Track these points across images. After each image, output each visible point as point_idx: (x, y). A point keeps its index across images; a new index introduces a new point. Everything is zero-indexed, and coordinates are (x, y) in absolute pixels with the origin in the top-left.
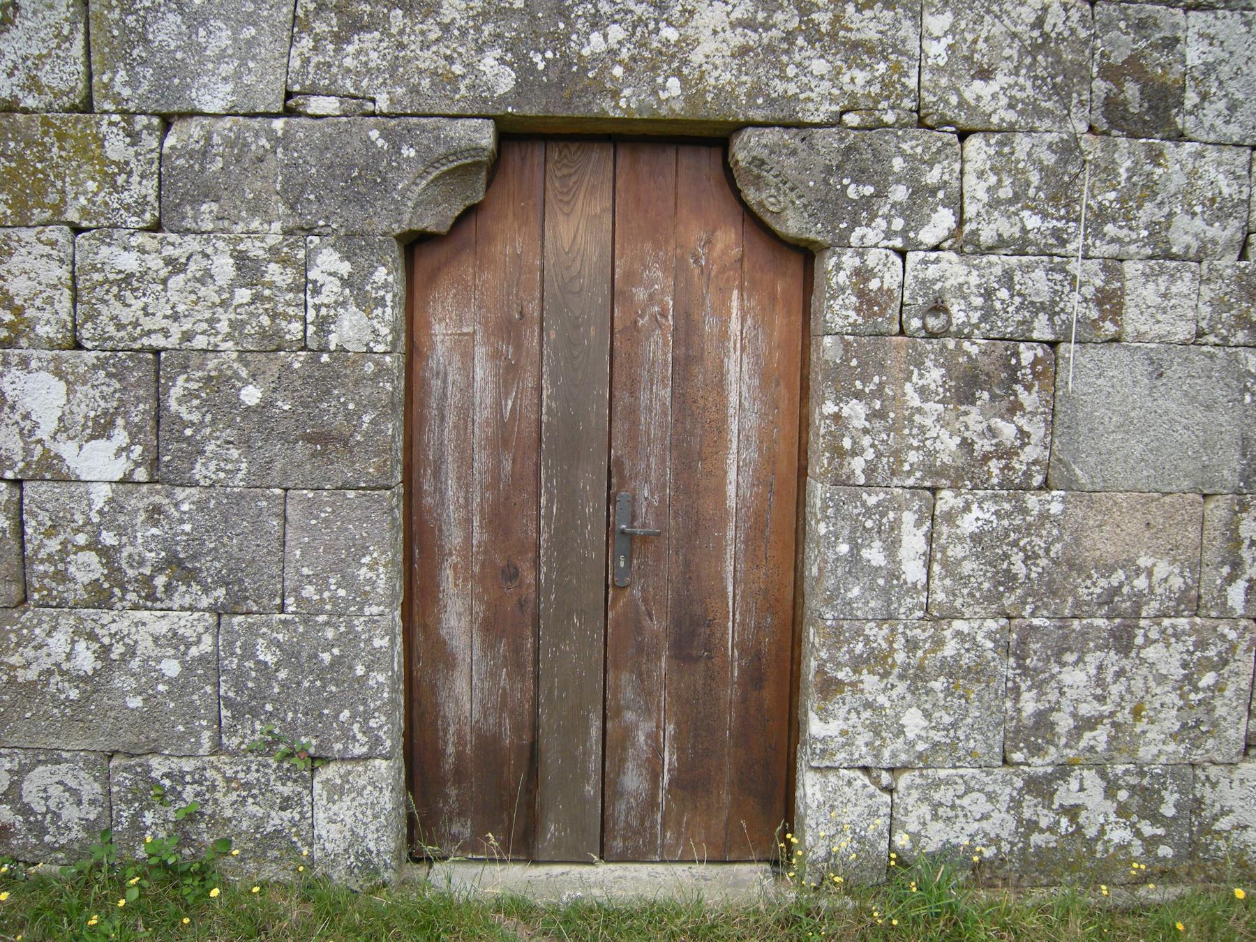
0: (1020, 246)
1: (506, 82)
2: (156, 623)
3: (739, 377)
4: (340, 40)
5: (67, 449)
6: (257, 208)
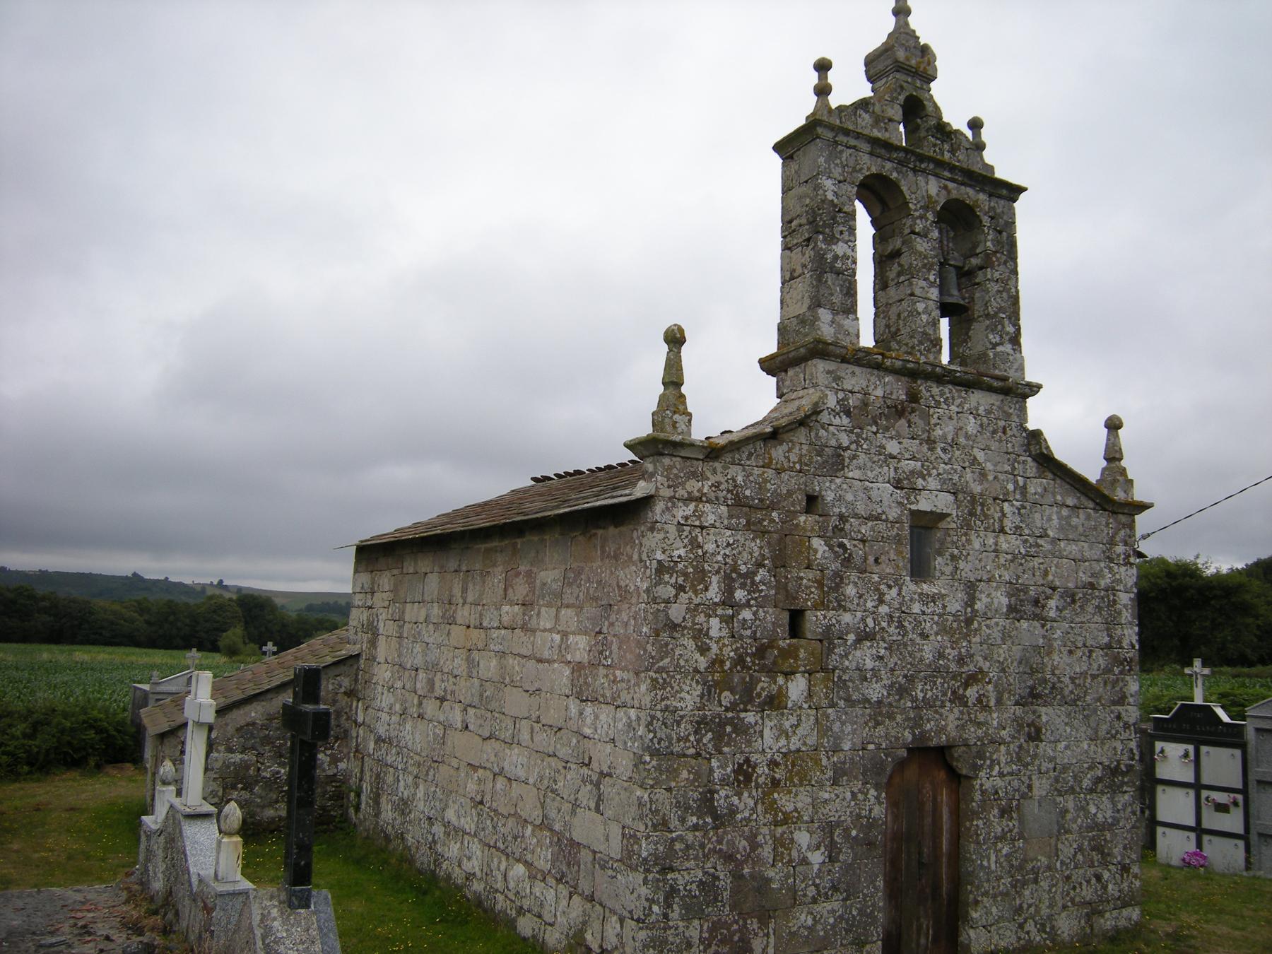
0: (1011, 774)
1: (910, 738)
2: (828, 906)
3: (945, 817)
4: (875, 728)
5: (809, 855)
6: (856, 778)
